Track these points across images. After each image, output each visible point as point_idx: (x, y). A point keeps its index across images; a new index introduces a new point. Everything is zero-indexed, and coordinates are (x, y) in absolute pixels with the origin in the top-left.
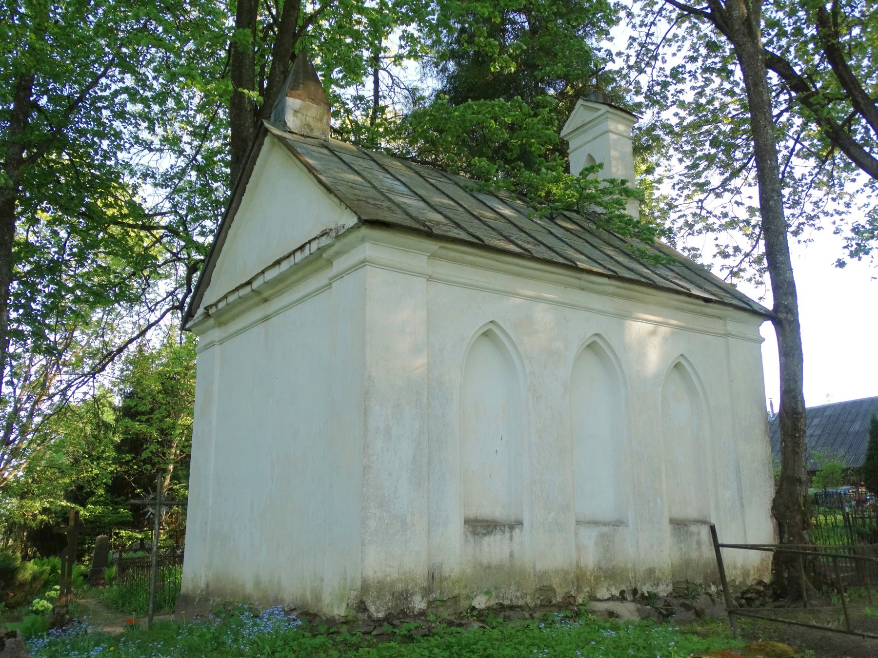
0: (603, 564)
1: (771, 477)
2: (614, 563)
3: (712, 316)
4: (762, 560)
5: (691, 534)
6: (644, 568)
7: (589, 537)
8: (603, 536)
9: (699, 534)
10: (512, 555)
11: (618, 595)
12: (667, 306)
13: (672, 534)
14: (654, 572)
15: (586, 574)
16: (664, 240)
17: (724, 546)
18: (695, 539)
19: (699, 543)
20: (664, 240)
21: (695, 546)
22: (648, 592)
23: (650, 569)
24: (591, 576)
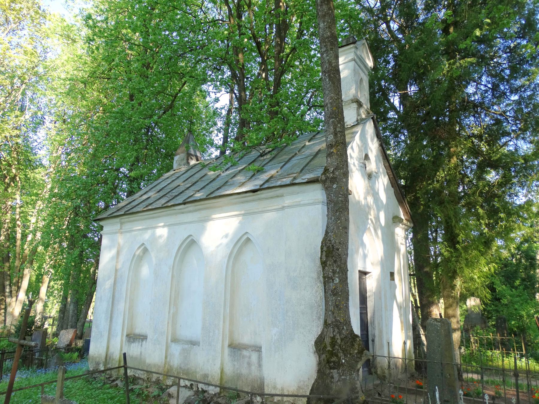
0: (182, 365)
1: (319, 318)
2: (189, 366)
3: (272, 198)
4: (299, 387)
5: (244, 357)
6: (201, 373)
7: (176, 350)
8: (183, 350)
9: (250, 357)
10: (141, 354)
11: (189, 385)
12: (236, 204)
13: (229, 354)
14: (208, 377)
15: (173, 369)
16: (490, 363)
17: (131, 368)
18: (246, 360)
19: (249, 364)
20: (490, 363)
21: (245, 365)
22: (202, 389)
23: (205, 374)
24: (175, 371)
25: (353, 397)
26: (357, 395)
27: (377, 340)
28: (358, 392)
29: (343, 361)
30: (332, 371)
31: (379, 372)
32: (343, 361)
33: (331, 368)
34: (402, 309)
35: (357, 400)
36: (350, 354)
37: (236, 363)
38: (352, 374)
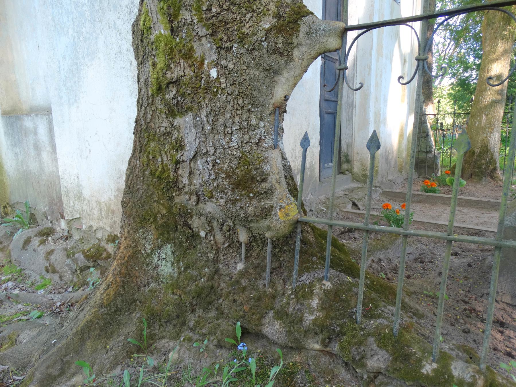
13: (5, 133)
25: (250, 210)
26: (266, 203)
27: (357, 111)
28: (269, 193)
29: (214, 73)
30: (177, 121)
31: (355, 170)
32: (214, 73)
33: (172, 113)
34: (407, 65)
35: (266, 223)
36: (242, 39)
37: (18, 150)
38: (251, 128)
